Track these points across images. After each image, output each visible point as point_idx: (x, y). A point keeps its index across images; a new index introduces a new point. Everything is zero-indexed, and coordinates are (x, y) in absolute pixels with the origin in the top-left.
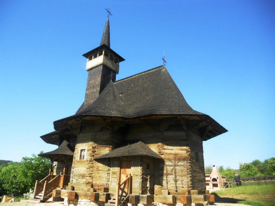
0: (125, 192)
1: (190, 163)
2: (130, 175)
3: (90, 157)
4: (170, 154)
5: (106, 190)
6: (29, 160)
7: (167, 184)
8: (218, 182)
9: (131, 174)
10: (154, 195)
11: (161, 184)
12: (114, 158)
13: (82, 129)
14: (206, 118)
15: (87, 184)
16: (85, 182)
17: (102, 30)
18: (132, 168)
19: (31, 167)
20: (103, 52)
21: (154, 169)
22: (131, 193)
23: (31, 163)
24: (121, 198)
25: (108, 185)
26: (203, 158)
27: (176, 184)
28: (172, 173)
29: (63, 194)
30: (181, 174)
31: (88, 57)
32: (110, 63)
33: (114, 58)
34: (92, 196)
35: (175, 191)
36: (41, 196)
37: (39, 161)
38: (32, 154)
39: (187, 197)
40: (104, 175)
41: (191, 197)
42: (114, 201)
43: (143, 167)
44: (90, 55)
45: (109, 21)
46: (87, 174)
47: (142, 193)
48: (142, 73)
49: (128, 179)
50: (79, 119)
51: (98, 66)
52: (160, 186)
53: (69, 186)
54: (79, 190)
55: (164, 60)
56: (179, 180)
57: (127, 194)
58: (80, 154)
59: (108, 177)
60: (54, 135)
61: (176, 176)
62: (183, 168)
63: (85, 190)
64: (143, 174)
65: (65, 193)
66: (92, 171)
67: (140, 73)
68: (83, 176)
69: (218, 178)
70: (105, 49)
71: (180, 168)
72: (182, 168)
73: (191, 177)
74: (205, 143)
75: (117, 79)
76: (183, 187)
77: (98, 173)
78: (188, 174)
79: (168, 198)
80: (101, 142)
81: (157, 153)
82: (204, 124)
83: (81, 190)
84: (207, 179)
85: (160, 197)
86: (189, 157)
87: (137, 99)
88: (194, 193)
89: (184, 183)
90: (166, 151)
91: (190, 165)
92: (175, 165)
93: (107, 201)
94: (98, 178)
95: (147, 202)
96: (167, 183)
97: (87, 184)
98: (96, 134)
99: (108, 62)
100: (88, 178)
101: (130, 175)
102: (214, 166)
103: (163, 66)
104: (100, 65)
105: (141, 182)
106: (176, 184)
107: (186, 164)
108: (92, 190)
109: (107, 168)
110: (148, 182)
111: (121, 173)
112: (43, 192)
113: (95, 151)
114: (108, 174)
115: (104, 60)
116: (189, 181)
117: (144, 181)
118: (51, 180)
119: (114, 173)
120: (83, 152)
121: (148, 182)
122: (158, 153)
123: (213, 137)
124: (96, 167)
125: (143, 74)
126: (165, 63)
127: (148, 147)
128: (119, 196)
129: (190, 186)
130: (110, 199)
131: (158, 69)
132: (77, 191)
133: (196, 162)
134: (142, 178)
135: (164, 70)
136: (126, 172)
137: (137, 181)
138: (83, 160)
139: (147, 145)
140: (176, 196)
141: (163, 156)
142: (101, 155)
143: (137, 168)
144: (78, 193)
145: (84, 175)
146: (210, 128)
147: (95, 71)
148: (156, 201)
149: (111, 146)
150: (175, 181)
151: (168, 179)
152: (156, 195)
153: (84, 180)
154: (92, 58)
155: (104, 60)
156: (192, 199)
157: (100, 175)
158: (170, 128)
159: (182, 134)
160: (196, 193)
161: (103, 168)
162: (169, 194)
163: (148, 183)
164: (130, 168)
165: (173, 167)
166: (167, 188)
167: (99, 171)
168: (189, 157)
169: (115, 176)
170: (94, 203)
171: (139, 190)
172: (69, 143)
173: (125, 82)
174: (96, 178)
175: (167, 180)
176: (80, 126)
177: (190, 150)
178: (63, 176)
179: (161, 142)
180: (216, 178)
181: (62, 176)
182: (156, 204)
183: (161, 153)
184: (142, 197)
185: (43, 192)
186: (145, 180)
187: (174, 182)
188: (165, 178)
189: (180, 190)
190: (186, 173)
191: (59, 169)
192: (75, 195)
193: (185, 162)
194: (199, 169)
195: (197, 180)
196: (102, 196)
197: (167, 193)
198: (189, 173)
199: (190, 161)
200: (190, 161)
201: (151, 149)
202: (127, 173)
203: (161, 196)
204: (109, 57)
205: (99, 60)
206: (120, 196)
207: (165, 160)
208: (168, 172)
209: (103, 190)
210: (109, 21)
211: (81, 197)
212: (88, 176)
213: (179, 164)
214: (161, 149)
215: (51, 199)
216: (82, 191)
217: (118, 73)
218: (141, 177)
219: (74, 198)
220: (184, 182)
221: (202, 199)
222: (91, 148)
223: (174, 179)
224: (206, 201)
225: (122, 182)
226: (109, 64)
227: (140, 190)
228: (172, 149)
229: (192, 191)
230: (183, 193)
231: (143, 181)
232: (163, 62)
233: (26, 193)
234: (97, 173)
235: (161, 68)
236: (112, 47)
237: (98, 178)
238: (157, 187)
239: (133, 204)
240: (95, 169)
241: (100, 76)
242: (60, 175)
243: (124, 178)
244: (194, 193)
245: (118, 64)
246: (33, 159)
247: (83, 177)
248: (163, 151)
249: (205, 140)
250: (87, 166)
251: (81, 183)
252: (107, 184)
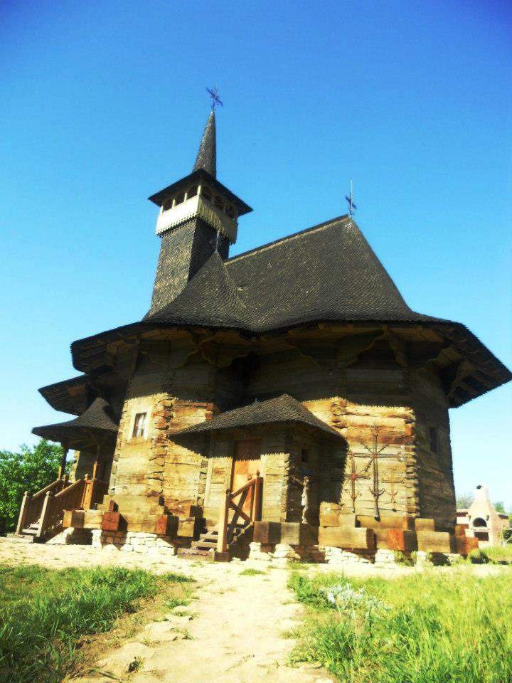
0: (244, 516)
1: (414, 450)
2: (258, 474)
3: (158, 432)
4: (362, 426)
5: (197, 512)
6: (13, 459)
7: (354, 501)
8: (489, 528)
9: (261, 472)
10: (320, 528)
11: (335, 498)
12: (219, 432)
13: (140, 362)
14: (456, 335)
15: (149, 496)
16: (146, 492)
17: (197, 139)
18: (262, 456)
19: (17, 474)
20: (199, 188)
21: (321, 462)
22: (259, 517)
23: (17, 465)
24: (231, 530)
25: (200, 501)
26: (449, 438)
27: (377, 501)
28: (367, 474)
29: (89, 519)
30: (390, 476)
31: (161, 202)
32: (215, 216)
33: (226, 204)
34: (160, 522)
35: (374, 520)
36: (36, 529)
37: (36, 461)
38: (21, 444)
39: (405, 532)
40: (191, 476)
41: (415, 536)
42: (213, 537)
43: (291, 456)
44: (165, 198)
45: (214, 117)
46: (150, 472)
47: (289, 519)
48: (295, 235)
49: (253, 484)
50: (135, 337)
51: (185, 222)
52: (335, 506)
53: (105, 502)
54: (130, 511)
55: (350, 201)
56: (384, 491)
57: (248, 520)
58: (135, 426)
59: (202, 482)
61: (376, 482)
62: (394, 462)
63: (142, 510)
64: (290, 473)
65: (95, 517)
66: (163, 466)
67: (289, 237)
68: (140, 478)
69: (488, 517)
70: (202, 179)
71: (389, 461)
72: (392, 462)
73: (416, 486)
74: (456, 416)
75: (231, 255)
76: (394, 510)
77: (177, 472)
78: (408, 479)
79: (357, 535)
80: (184, 393)
81: (328, 423)
82: (448, 355)
83: (135, 511)
84: (460, 520)
85: (334, 533)
86: (413, 434)
87: (279, 296)
88: (423, 527)
89: (399, 499)
90: (351, 419)
91: (414, 457)
92: (376, 456)
93: (196, 538)
94: (176, 482)
95: (301, 538)
96: (354, 499)
97: (149, 496)
98: (174, 376)
99: (211, 213)
100: (151, 482)
101: (258, 474)
102: (479, 487)
103: (347, 216)
104: (191, 219)
105: (285, 493)
106: (377, 501)
107: (404, 452)
108: (161, 511)
109: (199, 459)
110: (304, 495)
111: (235, 472)
112: (41, 520)
113: (172, 417)
114: (203, 475)
115: (200, 209)
116: (411, 495)
117: (293, 491)
118: (63, 491)
119: (217, 472)
120: (141, 421)
121: (304, 495)
122: (330, 424)
123: (475, 397)
124: (173, 457)
125: (297, 237)
126: (352, 209)
127: (307, 410)
128: (227, 525)
129: (415, 507)
130: (205, 532)
131: (335, 223)
132: (123, 514)
133: (429, 451)
134: (289, 482)
135: (350, 225)
136: (247, 470)
137: (275, 490)
138: (139, 439)
139: (305, 403)
140: (376, 531)
141: (343, 432)
142: (186, 427)
143: (276, 456)
144: (127, 517)
145: (143, 475)
146: (467, 368)
147: (177, 235)
148: (325, 543)
149: (211, 405)
150: (375, 495)
151: (356, 488)
152: (325, 527)
153: (142, 488)
154: (171, 204)
155: (201, 209)
156: (418, 539)
157: (182, 476)
158: (363, 360)
159: (393, 377)
160: (429, 527)
161: (189, 458)
162: (358, 524)
163: (303, 496)
164: (258, 458)
165: (369, 459)
166: (354, 512)
167: (179, 466)
168: (413, 434)
169: (219, 479)
170: (167, 541)
171: (280, 511)
172: (109, 402)
173: (253, 260)
174: (171, 482)
175: (353, 490)
176: (135, 355)
177: (414, 418)
178: (92, 483)
179: (341, 395)
180: (485, 518)
181: (89, 481)
182: (324, 549)
183: (339, 423)
184: (288, 528)
185: (41, 520)
186: (296, 487)
187: (372, 498)
188: (347, 485)
189: (387, 517)
190: (404, 475)
191: (83, 469)
192: (118, 520)
193: (402, 446)
194: (440, 471)
195: (432, 496)
196: (184, 523)
197: (354, 523)
198: (413, 475)
199: (414, 447)
200: (414, 447)
201: (314, 414)
202: (250, 472)
203: (337, 530)
204: (213, 202)
205: (190, 207)
206: (229, 525)
207: (349, 442)
208: (357, 472)
209: (188, 512)
210: (214, 117)
211: (132, 527)
212: (152, 476)
213: (387, 451)
214: (339, 413)
215: (61, 538)
216: (137, 512)
217: (235, 242)
218: (287, 478)
219: (115, 527)
220: (397, 498)
221: (446, 542)
222: (160, 408)
223: (372, 488)
224: (456, 552)
225: (237, 488)
226: (213, 217)
227: (282, 512)
228: (367, 415)
229: (419, 521)
230: (395, 526)
231: (289, 490)
232: (349, 205)
234: (175, 470)
235: (342, 221)
236: (223, 177)
237: (176, 482)
238: (326, 508)
239: (264, 542)
240: (171, 461)
241: (190, 246)
242: (86, 479)
243: (241, 482)
244: (423, 527)
245: (236, 220)
246: (21, 458)
247: (138, 480)
248: (345, 417)
249: (456, 404)
250: (151, 454)
251: (133, 493)
252: (199, 498)
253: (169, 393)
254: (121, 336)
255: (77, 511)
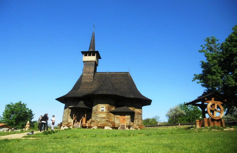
15: (107, 121)
60: (188, 105)
68: (104, 118)
92: (138, 116)
97: (107, 121)
109: (114, 115)
153: (105, 120)
157: (112, 118)
188: (135, 120)
222: (107, 107)
233: (16, 130)
253: (109, 104)
254: (43, 122)
255: (74, 115)
